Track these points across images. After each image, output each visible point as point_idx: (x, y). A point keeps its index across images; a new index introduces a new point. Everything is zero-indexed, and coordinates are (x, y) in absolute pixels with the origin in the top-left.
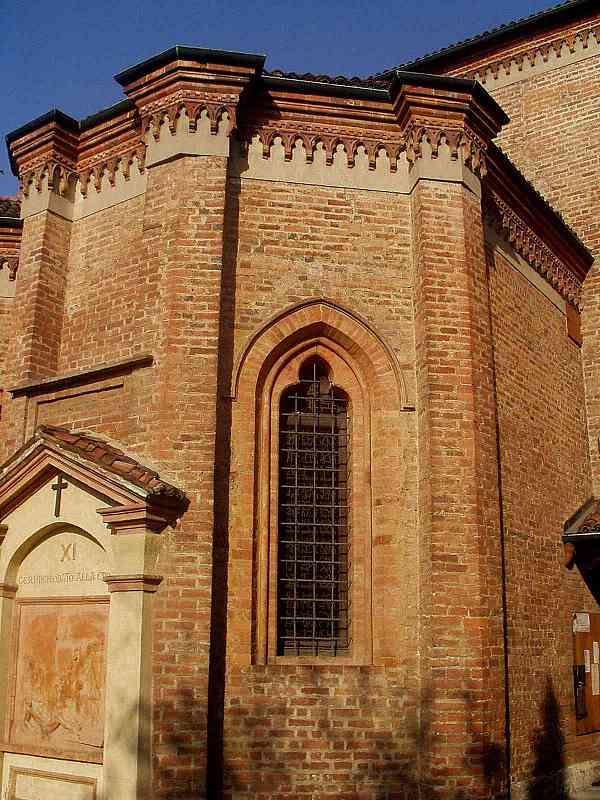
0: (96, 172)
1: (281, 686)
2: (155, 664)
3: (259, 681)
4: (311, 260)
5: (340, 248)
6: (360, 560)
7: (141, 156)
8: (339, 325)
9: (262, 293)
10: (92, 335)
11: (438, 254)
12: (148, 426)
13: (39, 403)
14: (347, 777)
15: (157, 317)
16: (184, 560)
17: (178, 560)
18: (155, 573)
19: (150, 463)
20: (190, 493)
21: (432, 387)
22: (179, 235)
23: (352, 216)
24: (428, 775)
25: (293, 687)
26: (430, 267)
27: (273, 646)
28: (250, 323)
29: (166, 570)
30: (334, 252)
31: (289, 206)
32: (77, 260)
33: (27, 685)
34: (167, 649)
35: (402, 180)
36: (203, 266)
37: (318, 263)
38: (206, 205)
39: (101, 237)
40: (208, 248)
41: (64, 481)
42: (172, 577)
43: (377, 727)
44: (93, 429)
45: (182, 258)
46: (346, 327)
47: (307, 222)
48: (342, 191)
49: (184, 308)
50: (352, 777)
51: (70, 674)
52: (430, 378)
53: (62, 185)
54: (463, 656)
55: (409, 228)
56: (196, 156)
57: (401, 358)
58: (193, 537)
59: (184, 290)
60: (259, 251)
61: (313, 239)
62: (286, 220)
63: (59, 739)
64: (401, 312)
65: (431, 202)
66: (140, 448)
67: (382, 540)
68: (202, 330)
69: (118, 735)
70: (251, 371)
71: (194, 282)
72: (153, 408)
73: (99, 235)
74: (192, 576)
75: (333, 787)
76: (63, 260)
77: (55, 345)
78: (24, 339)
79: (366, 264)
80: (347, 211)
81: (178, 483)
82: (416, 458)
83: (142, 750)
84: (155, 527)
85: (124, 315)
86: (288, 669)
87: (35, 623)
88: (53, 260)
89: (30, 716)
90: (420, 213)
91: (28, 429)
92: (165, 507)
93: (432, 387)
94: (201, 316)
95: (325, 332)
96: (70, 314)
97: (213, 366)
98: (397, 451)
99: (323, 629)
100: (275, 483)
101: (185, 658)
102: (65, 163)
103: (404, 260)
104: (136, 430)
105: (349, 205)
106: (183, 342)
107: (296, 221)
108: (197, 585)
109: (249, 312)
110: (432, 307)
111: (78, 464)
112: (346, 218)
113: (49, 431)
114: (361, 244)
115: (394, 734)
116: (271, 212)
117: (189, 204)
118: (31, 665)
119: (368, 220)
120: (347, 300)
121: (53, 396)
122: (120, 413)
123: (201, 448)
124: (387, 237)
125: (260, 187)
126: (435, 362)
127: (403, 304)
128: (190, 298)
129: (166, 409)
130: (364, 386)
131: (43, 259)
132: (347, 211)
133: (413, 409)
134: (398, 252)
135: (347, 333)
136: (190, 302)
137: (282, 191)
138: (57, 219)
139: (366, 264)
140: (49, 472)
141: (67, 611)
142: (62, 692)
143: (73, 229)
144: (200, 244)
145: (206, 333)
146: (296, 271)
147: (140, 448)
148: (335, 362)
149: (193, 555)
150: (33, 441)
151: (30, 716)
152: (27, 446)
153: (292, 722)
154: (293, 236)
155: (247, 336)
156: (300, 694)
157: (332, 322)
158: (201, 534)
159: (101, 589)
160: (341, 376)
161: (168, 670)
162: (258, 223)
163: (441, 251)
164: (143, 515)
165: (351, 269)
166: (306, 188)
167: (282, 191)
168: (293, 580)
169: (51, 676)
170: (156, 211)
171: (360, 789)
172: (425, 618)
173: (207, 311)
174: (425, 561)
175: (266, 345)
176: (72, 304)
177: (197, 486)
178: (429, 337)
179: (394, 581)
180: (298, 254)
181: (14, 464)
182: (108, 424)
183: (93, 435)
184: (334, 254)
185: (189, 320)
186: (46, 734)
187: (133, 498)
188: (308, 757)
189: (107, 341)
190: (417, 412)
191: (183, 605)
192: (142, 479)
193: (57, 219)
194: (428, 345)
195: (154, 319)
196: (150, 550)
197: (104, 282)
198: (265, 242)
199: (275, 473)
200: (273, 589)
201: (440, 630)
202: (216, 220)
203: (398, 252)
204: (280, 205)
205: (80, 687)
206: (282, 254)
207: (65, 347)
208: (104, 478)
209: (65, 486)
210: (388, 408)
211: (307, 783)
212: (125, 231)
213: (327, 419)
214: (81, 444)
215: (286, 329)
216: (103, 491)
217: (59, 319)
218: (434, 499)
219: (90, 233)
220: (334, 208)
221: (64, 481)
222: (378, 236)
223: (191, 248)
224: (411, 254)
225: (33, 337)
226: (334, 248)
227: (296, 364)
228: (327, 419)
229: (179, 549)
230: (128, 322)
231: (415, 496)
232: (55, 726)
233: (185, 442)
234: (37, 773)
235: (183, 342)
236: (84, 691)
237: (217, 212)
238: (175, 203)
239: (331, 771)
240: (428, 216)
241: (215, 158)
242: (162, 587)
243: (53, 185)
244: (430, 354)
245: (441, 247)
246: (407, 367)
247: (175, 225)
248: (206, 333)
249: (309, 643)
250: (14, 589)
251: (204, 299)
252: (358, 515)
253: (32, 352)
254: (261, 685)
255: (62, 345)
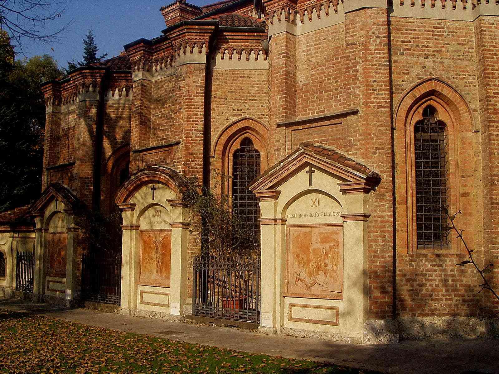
0: (309, 11)
1: (421, 263)
2: (371, 256)
3: (411, 261)
4: (427, 58)
5: (440, 51)
6: (454, 204)
7: (335, 3)
8: (442, 90)
9: (404, 76)
10: (315, 96)
11: (490, 54)
12: (358, 143)
13: (292, 130)
14: (451, 305)
15: (359, 90)
16: (380, 206)
17: (377, 206)
18: (367, 213)
19: (362, 161)
20: (382, 174)
21: (490, 122)
22: (366, 49)
23: (445, 34)
24: (489, 304)
25: (426, 264)
26: (487, 61)
27: (415, 245)
28: (400, 91)
29: (372, 211)
30: (438, 53)
31: (415, 30)
32: (301, 56)
33: (296, 266)
34: (374, 247)
35: (469, 15)
36: (380, 65)
37: (430, 59)
38: (379, 34)
39: (315, 45)
40: (381, 56)
41: (313, 169)
42: (375, 214)
43: (464, 282)
44: (326, 144)
45: (369, 61)
46: (445, 91)
47: (424, 38)
48: (440, 21)
49: (372, 86)
50: (453, 305)
51: (320, 260)
52: (488, 117)
53: (291, 17)
54: (8, 235)
55: (474, 39)
56: (371, 8)
57: (472, 106)
58: (384, 196)
59: (372, 77)
60: (402, 54)
61: (427, 47)
62: (414, 38)
63: (315, 289)
64: (471, 83)
65: (486, 27)
66: (355, 154)
67: (465, 195)
68: (382, 96)
69: (355, 285)
70: (402, 114)
71: (377, 73)
72: (360, 134)
73: (313, 44)
74: (384, 214)
75: (445, 309)
76: (294, 56)
77: (294, 100)
78: (280, 99)
79: (453, 59)
80: (443, 32)
81: (376, 170)
82: (480, 155)
83: (367, 292)
84: (366, 191)
85: (333, 86)
86: (425, 255)
87: (298, 237)
88: (289, 56)
89: (299, 279)
90: (480, 33)
91: (287, 143)
92: (373, 182)
93: (490, 122)
94: (381, 90)
95: (435, 94)
96: (300, 84)
97: (388, 114)
98: (471, 152)
99: (437, 237)
100: (414, 168)
101: (383, 251)
102: (292, 6)
103: (472, 56)
104: (352, 145)
105: (444, 28)
106: (373, 103)
107: (418, 38)
108: (387, 218)
109: (399, 85)
110: (488, 81)
111: (325, 162)
112: (442, 35)
113: (306, 145)
114: (451, 48)
115: (472, 285)
116: (406, 34)
117: (370, 34)
118: (298, 256)
119: (453, 36)
120: (445, 78)
121: (301, 127)
122: (341, 136)
123: (386, 154)
124: (463, 44)
125: (400, 21)
126: (491, 109)
127: (472, 78)
128: (374, 81)
129: (367, 135)
130: (454, 120)
131: (286, 57)
132: (443, 32)
133: (478, 131)
134: (468, 52)
135: (446, 94)
136: (375, 83)
137: (410, 22)
138: (290, 34)
139: (453, 59)
140: (306, 164)
141: (316, 230)
142: (316, 268)
143: (297, 40)
144: (377, 53)
145: (384, 98)
146: (420, 64)
147: (355, 154)
148: (439, 108)
149: (384, 204)
150: (298, 150)
151: (299, 279)
152: (295, 153)
153: (426, 280)
154: (417, 46)
155: (400, 96)
156: (429, 267)
157: (439, 89)
158: (387, 194)
159: (340, 220)
160: (442, 115)
161: (375, 256)
162: (400, 40)
163: (492, 53)
164: (363, 186)
165: (446, 62)
166: (422, 20)
167: (410, 22)
168: (238, 194)
169: (309, 261)
170: (352, 36)
171: (457, 310)
172: (487, 231)
173: (384, 88)
174: (487, 205)
175: (408, 102)
176: (301, 79)
177: (384, 172)
178: (487, 97)
179: (471, 214)
180: (420, 55)
181: (286, 161)
182: (334, 141)
183: (326, 147)
184: (438, 55)
185: (375, 92)
186: (308, 287)
187: (357, 178)
188: (433, 296)
189: (325, 99)
190: (480, 133)
191: (381, 227)
192: (362, 169)
193: (290, 34)
194: (487, 101)
195: (357, 91)
196: (365, 202)
197: (319, 69)
198: (404, 50)
199: (413, 163)
200: (415, 219)
201: (496, 237)
202: (384, 41)
203: (468, 52)
204: (411, 30)
205: (326, 265)
206: (413, 55)
207: (299, 101)
208: (341, 169)
209: (314, 172)
210: (467, 131)
211: (433, 307)
212: (330, 43)
213: (434, 136)
214: (321, 151)
215: (418, 93)
216: (339, 174)
217: (295, 88)
218: (491, 176)
219: (308, 43)
220: (437, 30)
221: (313, 169)
222: (459, 44)
223: (373, 56)
224: (475, 53)
225: (286, 97)
226: (438, 51)
227: (421, 110)
228: (434, 136)
229: (377, 201)
230: (336, 90)
231: (480, 173)
232: (313, 284)
233: (378, 151)
234: (303, 306)
235: (373, 103)
236: (330, 267)
237: (384, 37)
238: (363, 33)
239: (444, 302)
240: (485, 35)
241: (381, 9)
242: (370, 219)
243: (287, 18)
244: (488, 105)
245: (492, 51)
246: (475, 110)
247: (364, 44)
248: (384, 98)
249: (429, 243)
250: (285, 221)
251: (382, 81)
252: (452, 183)
253: (286, 105)
254: (412, 263)
255: (297, 100)
